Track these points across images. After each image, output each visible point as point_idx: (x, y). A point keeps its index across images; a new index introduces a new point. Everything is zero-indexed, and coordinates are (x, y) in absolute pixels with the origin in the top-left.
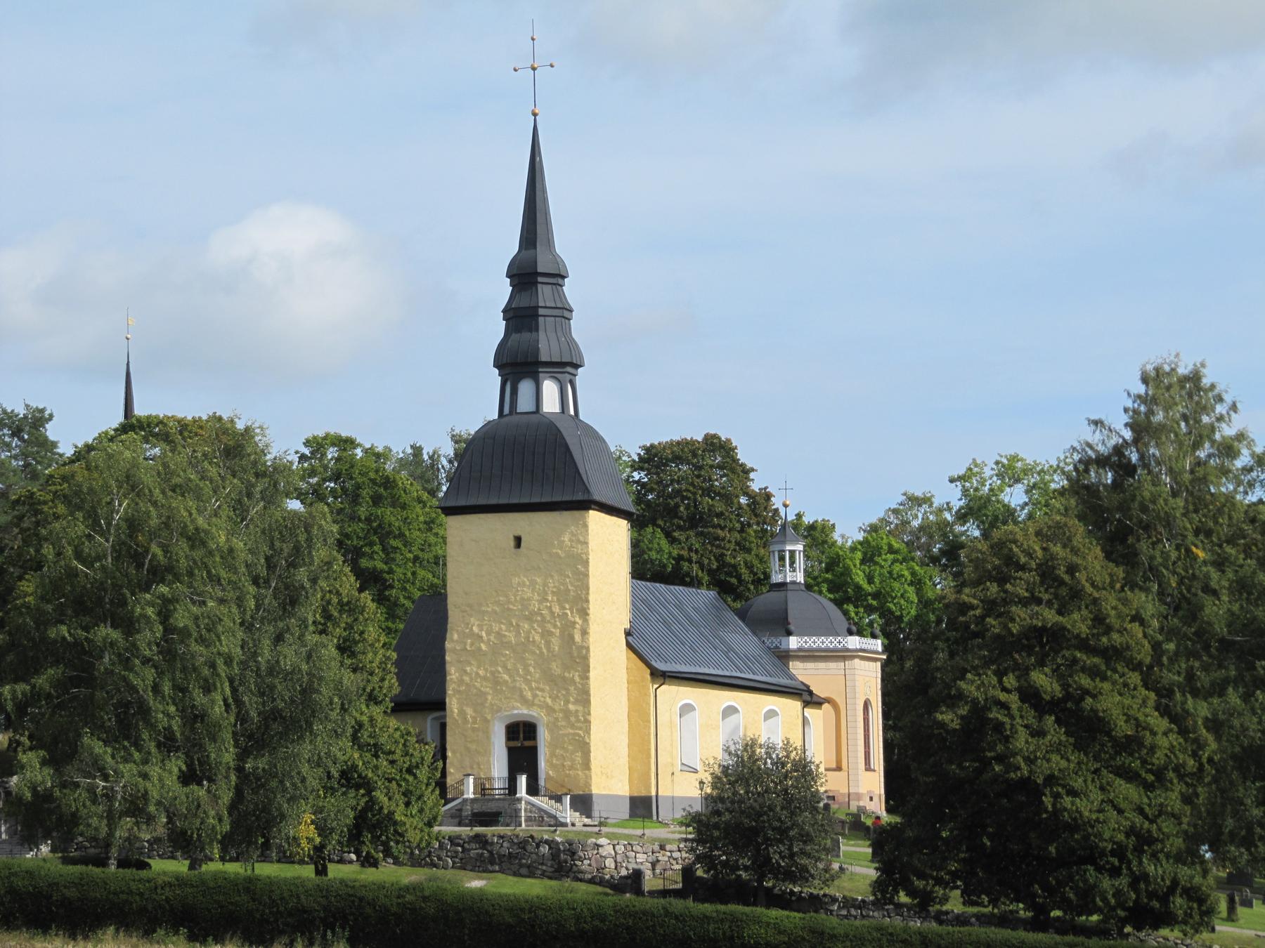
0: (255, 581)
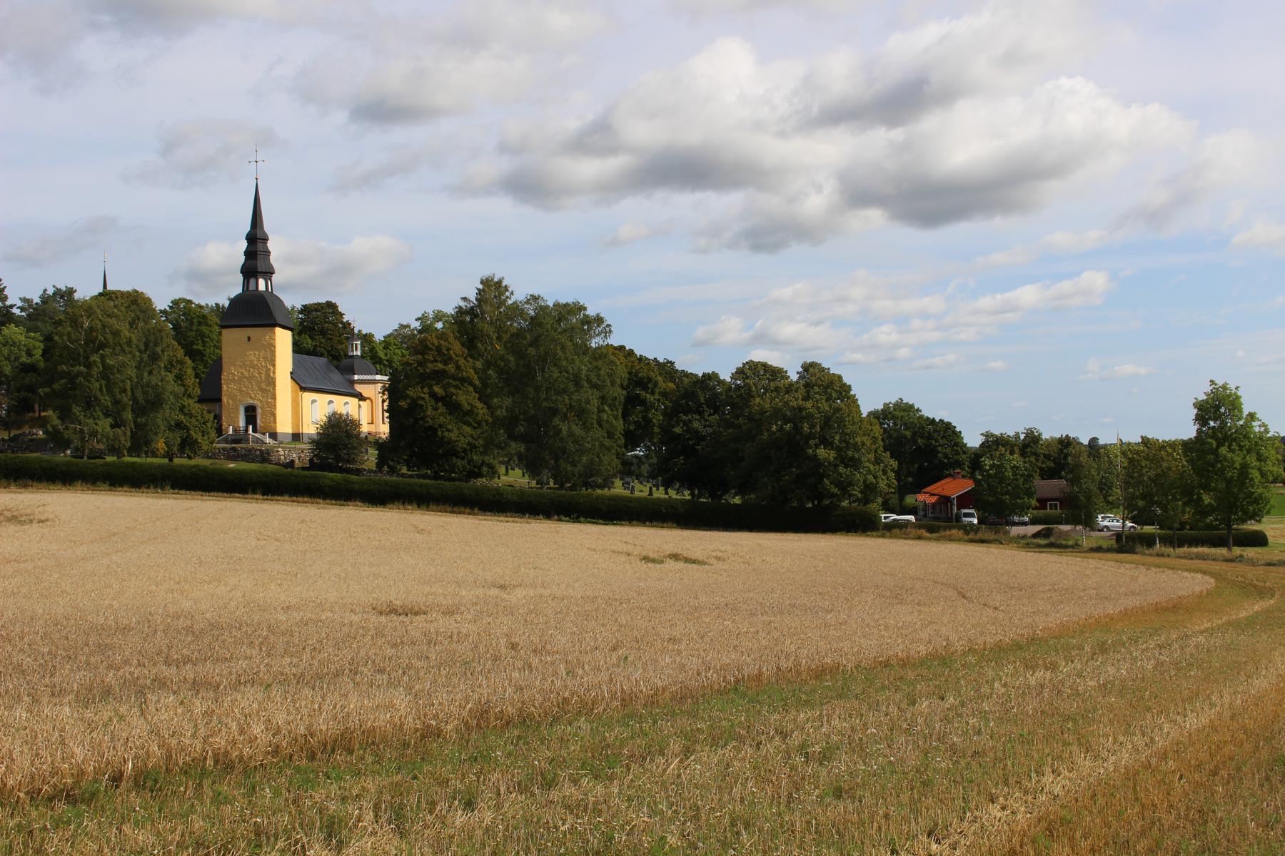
0: (140, 351)
